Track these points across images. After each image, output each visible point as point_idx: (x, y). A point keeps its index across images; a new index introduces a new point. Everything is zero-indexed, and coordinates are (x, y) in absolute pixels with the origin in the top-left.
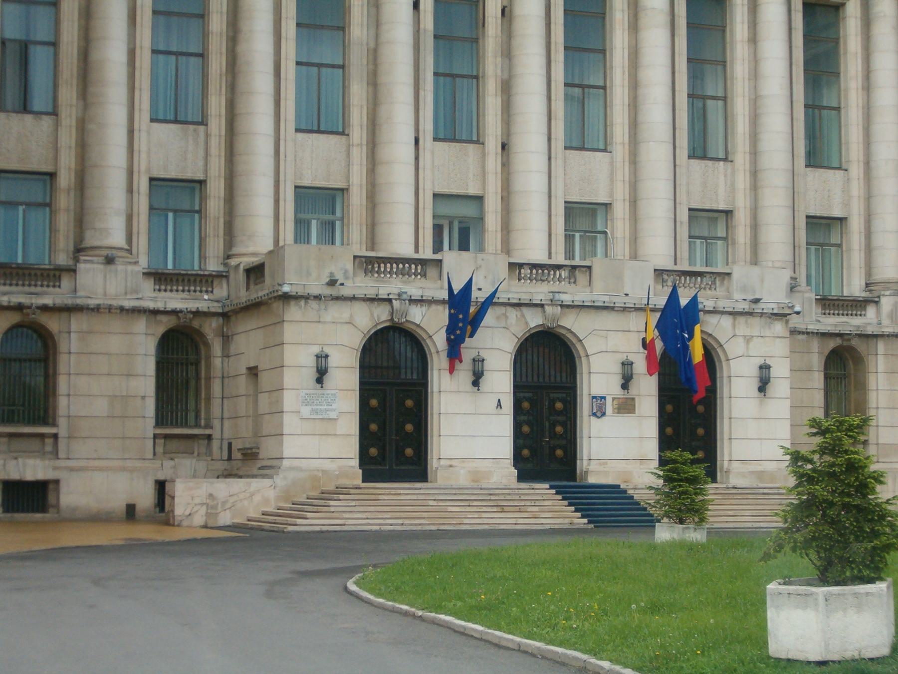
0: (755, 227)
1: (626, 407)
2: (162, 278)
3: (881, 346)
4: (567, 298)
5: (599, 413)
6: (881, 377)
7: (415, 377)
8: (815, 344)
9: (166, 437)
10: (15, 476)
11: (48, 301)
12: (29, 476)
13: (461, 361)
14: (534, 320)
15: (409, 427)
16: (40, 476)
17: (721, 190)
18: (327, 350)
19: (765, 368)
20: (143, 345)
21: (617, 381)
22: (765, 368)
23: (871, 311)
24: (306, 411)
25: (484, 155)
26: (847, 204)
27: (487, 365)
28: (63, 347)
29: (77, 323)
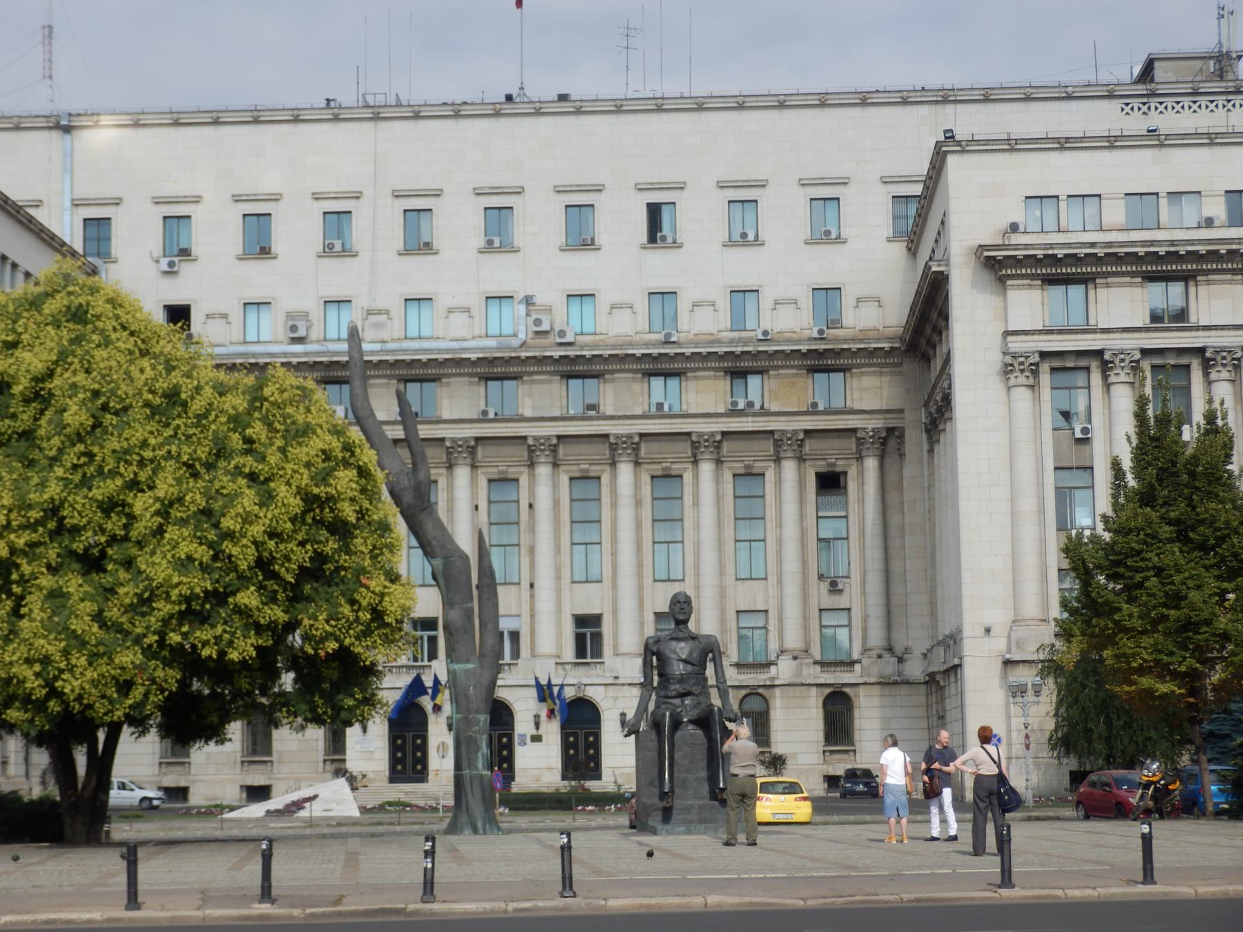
0: (781, 620)
1: (537, 739)
2: (823, 664)
3: (777, 691)
5: (523, 743)
6: (778, 711)
9: (832, 752)
10: (249, 783)
12: (256, 783)
13: (623, 715)
15: (419, 754)
16: (262, 783)
20: (815, 701)
21: (532, 725)
23: (773, 668)
24: (358, 747)
26: (767, 602)
28: (856, 704)
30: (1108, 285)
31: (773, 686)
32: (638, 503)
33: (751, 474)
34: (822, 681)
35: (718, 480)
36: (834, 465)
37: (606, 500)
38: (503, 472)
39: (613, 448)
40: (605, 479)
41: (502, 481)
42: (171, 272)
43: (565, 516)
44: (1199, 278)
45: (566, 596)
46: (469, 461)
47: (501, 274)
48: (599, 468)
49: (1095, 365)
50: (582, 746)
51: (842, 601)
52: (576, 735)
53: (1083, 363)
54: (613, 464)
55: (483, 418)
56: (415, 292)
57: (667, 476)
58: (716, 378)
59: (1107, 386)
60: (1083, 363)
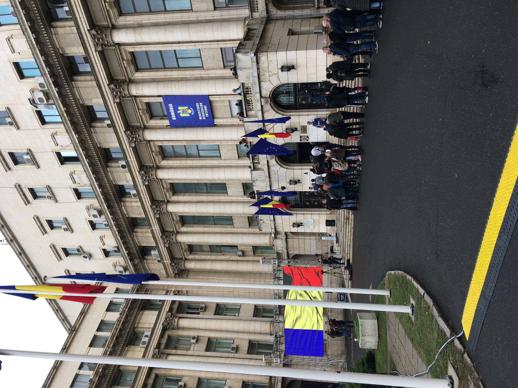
18: (280, 67)
19: (283, 69)
22: (283, 69)
24: (311, 227)
30: (139, 323)
44: (135, 326)
49: (169, 333)
53: (166, 337)
59: (178, 328)
60: (166, 337)
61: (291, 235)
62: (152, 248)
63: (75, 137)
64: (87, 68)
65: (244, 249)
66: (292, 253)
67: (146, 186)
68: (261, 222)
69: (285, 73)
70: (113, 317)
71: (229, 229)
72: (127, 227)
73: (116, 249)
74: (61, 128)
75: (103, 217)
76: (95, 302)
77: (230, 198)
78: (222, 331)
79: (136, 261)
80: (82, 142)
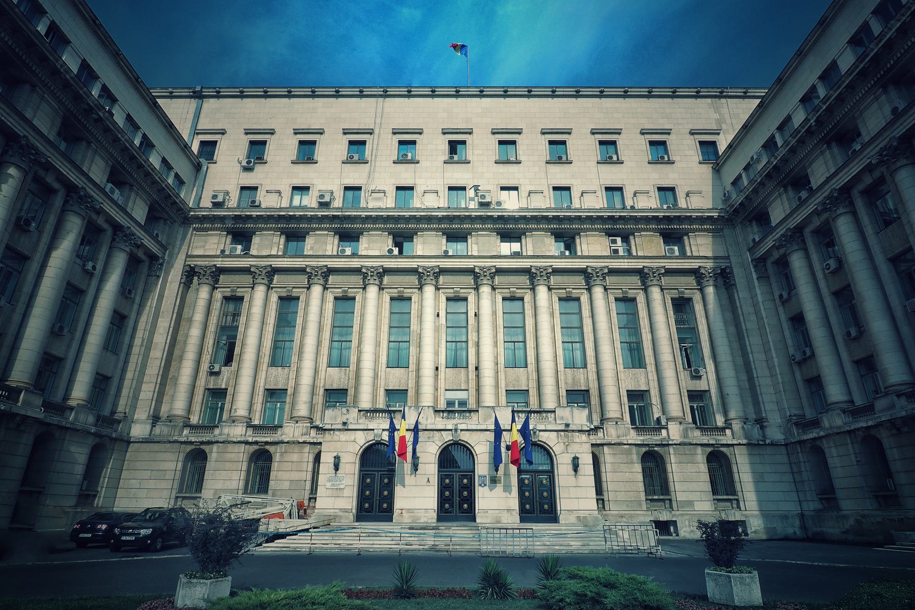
4: (460, 427)
7: (172, 466)
8: (634, 449)
11: (268, 439)
12: (731, 519)
14: (448, 437)
17: (582, 381)
18: (340, 454)
20: (700, 456)
24: (329, 485)
25: (118, 360)
27: (580, 462)
29: (215, 448)
31: (668, 445)
32: (552, 314)
33: (400, 299)
34: (705, 442)
35: (437, 299)
36: (683, 293)
37: (529, 312)
38: (457, 292)
39: (365, 276)
40: (528, 298)
41: (400, 299)
42: (248, 169)
43: (500, 322)
45: (502, 376)
46: (377, 282)
47: (458, 175)
48: (522, 291)
50: (377, 486)
51: (701, 385)
52: (450, 477)
54: (477, 289)
55: (446, 255)
56: (454, 183)
57: (512, 299)
58: (601, 236)
61: (317, 451)
62: (247, 248)
63: (440, 214)
64: (348, 251)
65: (221, 377)
66: (214, 453)
67: (361, 268)
68: (344, 410)
69: (569, 461)
70: (155, 160)
71: (266, 360)
72: (294, 229)
73: (257, 204)
74: (285, 203)
75: (210, 205)
76: (368, 146)
77: (324, 369)
78: (593, 316)
79: (229, 225)
80: (429, 219)
